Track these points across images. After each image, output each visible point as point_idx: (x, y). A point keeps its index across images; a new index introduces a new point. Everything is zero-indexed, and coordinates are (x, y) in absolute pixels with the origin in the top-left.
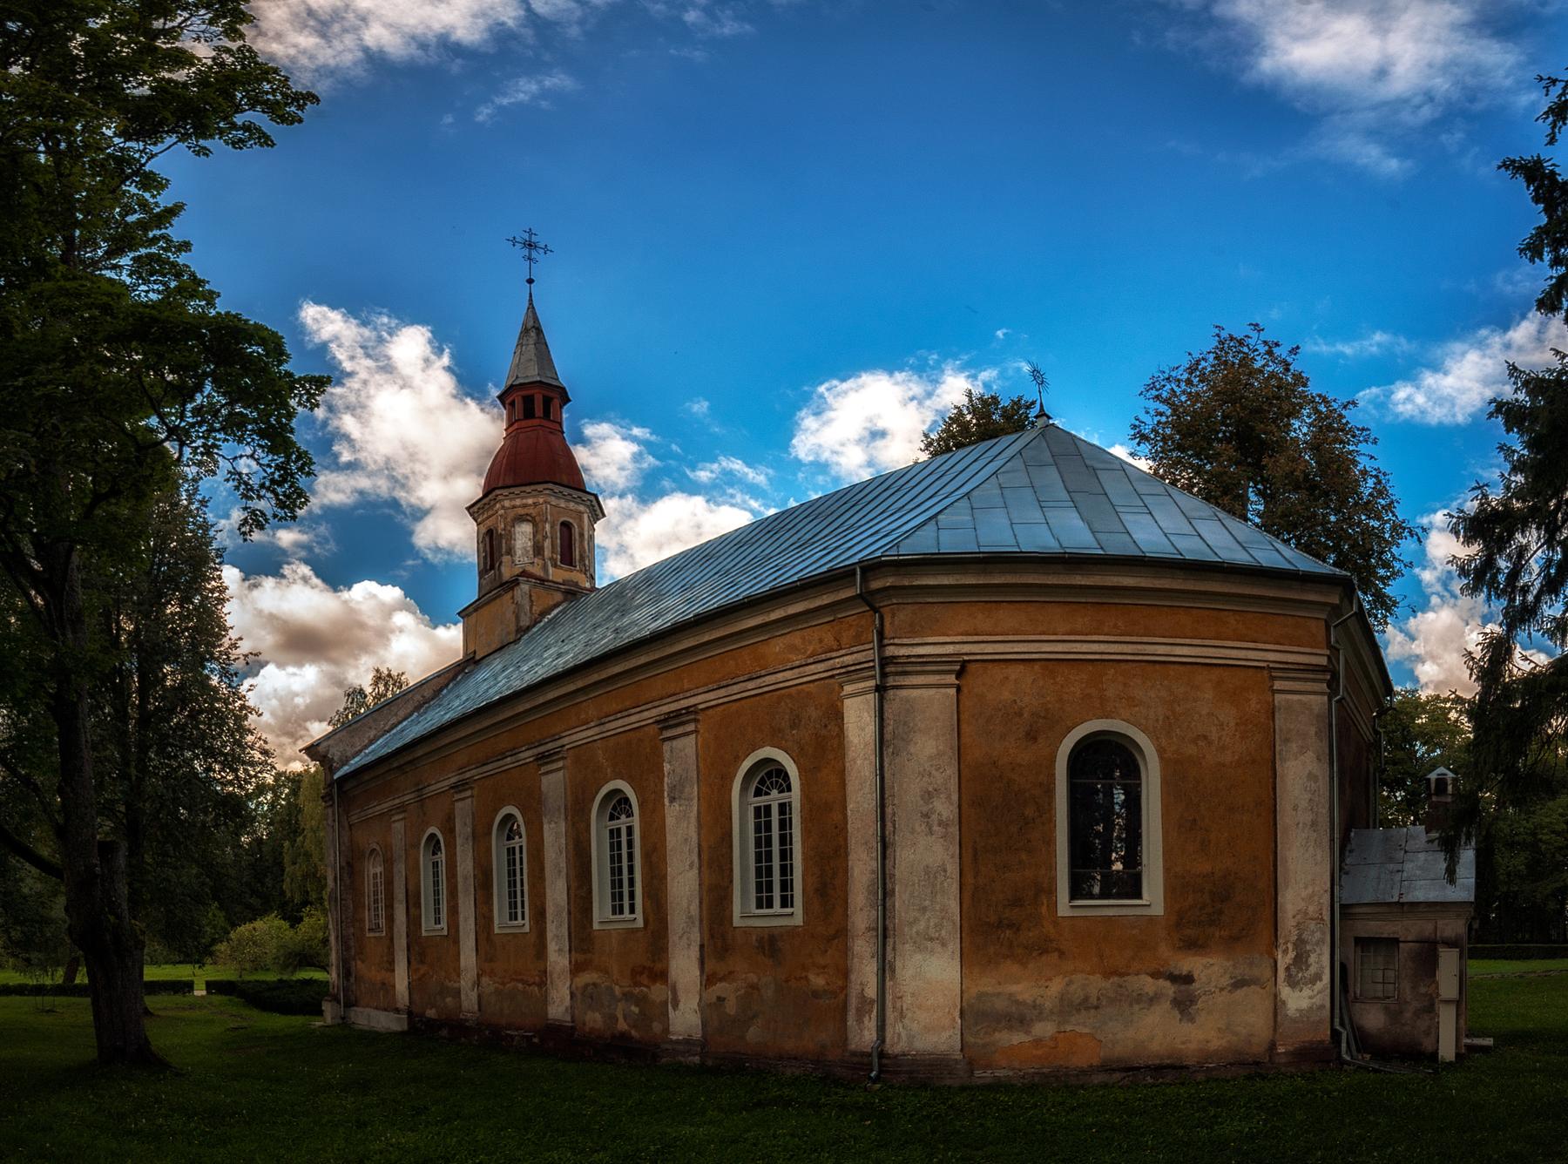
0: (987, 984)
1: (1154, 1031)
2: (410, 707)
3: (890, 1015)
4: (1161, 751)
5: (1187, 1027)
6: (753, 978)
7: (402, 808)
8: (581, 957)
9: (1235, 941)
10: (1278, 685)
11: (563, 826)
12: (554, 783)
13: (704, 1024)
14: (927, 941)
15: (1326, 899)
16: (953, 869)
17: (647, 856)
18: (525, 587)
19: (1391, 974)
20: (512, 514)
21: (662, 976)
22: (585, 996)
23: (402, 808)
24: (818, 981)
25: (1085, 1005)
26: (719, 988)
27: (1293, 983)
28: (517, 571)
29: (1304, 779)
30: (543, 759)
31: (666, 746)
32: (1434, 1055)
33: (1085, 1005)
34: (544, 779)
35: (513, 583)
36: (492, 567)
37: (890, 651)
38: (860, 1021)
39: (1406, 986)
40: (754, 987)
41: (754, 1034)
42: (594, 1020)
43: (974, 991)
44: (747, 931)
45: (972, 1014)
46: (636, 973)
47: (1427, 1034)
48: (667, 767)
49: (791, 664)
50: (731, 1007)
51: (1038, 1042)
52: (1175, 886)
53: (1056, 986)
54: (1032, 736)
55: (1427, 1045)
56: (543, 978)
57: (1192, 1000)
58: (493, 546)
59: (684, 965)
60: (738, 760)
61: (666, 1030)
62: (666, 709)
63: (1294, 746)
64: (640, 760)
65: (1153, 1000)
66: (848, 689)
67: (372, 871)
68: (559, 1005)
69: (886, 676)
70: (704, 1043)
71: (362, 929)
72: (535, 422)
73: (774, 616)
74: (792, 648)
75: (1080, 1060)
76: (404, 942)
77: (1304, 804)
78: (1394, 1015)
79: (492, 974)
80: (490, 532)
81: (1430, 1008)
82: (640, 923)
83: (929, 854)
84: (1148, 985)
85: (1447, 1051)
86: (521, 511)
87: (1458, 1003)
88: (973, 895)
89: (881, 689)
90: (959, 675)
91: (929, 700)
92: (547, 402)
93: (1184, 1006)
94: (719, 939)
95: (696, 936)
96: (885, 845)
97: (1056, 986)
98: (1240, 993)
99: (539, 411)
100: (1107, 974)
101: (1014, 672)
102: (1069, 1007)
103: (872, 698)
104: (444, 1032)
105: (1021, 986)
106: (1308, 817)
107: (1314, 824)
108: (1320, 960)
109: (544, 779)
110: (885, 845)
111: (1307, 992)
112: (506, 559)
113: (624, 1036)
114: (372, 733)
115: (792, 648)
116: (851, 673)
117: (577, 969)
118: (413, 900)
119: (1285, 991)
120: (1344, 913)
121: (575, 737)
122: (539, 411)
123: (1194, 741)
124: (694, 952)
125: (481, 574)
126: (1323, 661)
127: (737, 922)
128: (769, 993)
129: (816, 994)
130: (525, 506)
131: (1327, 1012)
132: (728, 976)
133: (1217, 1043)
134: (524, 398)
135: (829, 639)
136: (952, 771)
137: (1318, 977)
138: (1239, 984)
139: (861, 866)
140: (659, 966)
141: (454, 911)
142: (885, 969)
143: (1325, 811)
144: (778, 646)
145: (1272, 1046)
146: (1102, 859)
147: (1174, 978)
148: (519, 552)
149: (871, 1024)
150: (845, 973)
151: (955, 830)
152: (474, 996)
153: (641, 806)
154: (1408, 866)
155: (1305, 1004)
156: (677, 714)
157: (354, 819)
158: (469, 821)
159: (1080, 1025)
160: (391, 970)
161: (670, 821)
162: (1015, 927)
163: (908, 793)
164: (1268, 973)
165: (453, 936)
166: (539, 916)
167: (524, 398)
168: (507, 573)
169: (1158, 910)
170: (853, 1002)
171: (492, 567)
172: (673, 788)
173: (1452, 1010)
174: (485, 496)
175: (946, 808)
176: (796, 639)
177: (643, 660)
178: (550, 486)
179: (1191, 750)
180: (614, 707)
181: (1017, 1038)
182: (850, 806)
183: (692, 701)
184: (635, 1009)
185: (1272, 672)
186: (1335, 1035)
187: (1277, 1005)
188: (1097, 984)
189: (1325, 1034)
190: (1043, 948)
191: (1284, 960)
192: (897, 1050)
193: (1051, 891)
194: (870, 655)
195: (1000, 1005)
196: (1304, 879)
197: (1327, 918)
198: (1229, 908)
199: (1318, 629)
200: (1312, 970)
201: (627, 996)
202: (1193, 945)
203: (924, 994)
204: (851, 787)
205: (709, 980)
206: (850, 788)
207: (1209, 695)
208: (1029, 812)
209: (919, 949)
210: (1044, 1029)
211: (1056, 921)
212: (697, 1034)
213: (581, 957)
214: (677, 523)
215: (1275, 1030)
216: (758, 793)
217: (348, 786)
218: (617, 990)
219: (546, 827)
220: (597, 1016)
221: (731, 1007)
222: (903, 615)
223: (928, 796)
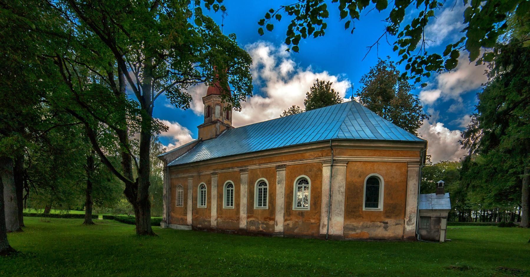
0: (348, 222)
1: (380, 232)
2: (186, 150)
3: (330, 228)
4: (384, 180)
5: (386, 232)
7: (192, 177)
8: (250, 215)
9: (396, 216)
10: (409, 166)
11: (247, 186)
12: (244, 177)
13: (284, 229)
14: (338, 214)
15: (416, 209)
16: (343, 201)
17: (270, 195)
18: (219, 124)
19: (428, 224)
20: (215, 102)
21: (273, 219)
22: (250, 223)
23: (192, 177)
24: (313, 221)
25: (367, 227)
26: (288, 222)
27: (408, 225)
28: (216, 119)
29: (413, 185)
30: (241, 171)
31: (278, 172)
32: (439, 241)
33: (367, 227)
34: (242, 176)
35: (215, 122)
36: (209, 116)
37: (335, 158)
38: (323, 228)
39: (432, 227)
40: (296, 222)
41: (296, 231)
42: (253, 228)
43: (346, 224)
44: (295, 211)
45: (345, 228)
46: (265, 219)
47: (437, 236)
48: (277, 177)
49: (311, 160)
50: (291, 226)
51: (357, 234)
52: (385, 205)
53: (361, 223)
54: (360, 176)
55: (437, 238)
56: (238, 219)
57: (387, 227)
58: (209, 111)
59: (280, 217)
60: (295, 177)
61: (274, 230)
62: (278, 164)
63: (411, 178)
64: (271, 175)
65: (380, 227)
66: (324, 165)
67: (178, 191)
68: (243, 224)
69: (333, 163)
70: (284, 233)
71: (174, 205)
73: (309, 148)
74: (311, 155)
75: (365, 237)
76: (191, 209)
77: (412, 190)
78: (429, 232)
79: (221, 217)
80: (209, 106)
81: (438, 231)
82: (267, 208)
83: (339, 198)
84: (379, 224)
85: (442, 239)
86: (217, 102)
87: (445, 230)
88: (347, 206)
89: (332, 166)
90: (347, 164)
91: (341, 169)
93: (386, 228)
94: (288, 211)
95: (283, 211)
96: (331, 196)
97: (361, 223)
98: (397, 226)
100: (371, 222)
101: (358, 164)
102: (363, 227)
103: (330, 167)
104: (205, 230)
105: (354, 223)
106: (413, 193)
107: (415, 194)
108: (414, 220)
109: (242, 176)
110: (331, 196)
111: (411, 226)
112: (213, 115)
113: (261, 231)
114: (177, 155)
115: (311, 155)
116: (325, 162)
117: (248, 217)
118: (195, 199)
119: (406, 226)
120: (420, 211)
123: (391, 178)
124: (282, 215)
125: (205, 117)
126: (419, 160)
127: (293, 209)
128: (301, 223)
129: (312, 224)
131: (415, 231)
132: (291, 220)
133: (391, 235)
135: (320, 154)
136: (344, 183)
137: (413, 224)
138: (397, 224)
139: (325, 200)
140: (272, 217)
141: (209, 202)
142: (329, 219)
143: (417, 191)
144: (308, 154)
145: (403, 236)
146: (372, 199)
147: (384, 223)
148: (216, 114)
150: (320, 220)
151: (344, 194)
152: (216, 222)
153: (269, 184)
154: (433, 202)
155: (410, 229)
156: (282, 165)
157: (173, 177)
158: (216, 182)
159: (365, 231)
160: (186, 214)
161: (277, 188)
162: (354, 212)
163: (336, 186)
164: (403, 223)
165: (209, 209)
166: (238, 205)
168: (213, 119)
169: (382, 210)
170: (321, 225)
171: (209, 116)
172: (279, 181)
173: (444, 232)
175: (343, 190)
176: (312, 153)
177: (274, 153)
179: (390, 179)
180: (264, 162)
181: (353, 233)
182: (323, 188)
183: (285, 163)
184: (265, 226)
185: (408, 163)
186: (416, 235)
187: (404, 229)
188: (369, 223)
189: (414, 235)
190: (360, 216)
191: (406, 220)
192: (331, 234)
193: (362, 206)
194: (330, 159)
195: (351, 226)
196: (412, 204)
197: (416, 212)
198: (397, 210)
199: (418, 153)
200: (412, 222)
201: (263, 223)
202: (388, 217)
203: (335, 224)
204: (323, 184)
205: (285, 220)
206: (323, 185)
207: (395, 168)
208: (359, 191)
209: (336, 215)
210: (358, 231)
211: (362, 211)
212: (282, 231)
213: (250, 215)
215: (404, 233)
216: (299, 184)
217: (171, 168)
218: (260, 222)
219: (241, 186)
220: (254, 227)
221: (291, 226)
222: (337, 151)
223: (340, 187)
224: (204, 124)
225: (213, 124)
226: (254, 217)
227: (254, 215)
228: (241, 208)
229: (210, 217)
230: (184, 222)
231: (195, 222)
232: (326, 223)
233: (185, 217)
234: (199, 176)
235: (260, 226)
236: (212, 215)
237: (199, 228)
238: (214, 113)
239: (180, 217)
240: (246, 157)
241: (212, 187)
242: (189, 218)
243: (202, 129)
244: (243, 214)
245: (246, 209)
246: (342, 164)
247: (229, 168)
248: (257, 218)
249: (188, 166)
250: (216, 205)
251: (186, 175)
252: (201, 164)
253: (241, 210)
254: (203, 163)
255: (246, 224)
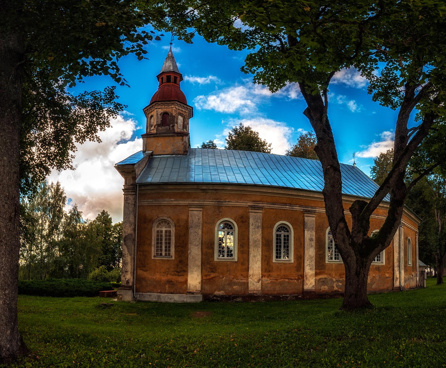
6: (374, 275)
8: (318, 271)
38: (396, 281)
40: (374, 277)
41: (374, 286)
42: (325, 288)
56: (302, 277)
68: (310, 283)
72: (171, 84)
92: (175, 78)
99: (172, 80)
104: (239, 299)
113: (336, 291)
117: (316, 274)
121: (321, 210)
122: (172, 80)
129: (387, 278)
130: (182, 111)
134: (167, 76)
149: (398, 282)
167: (167, 76)
174: (150, 105)
178: (177, 102)
201: (337, 281)
213: (318, 271)
214: (118, 97)
218: (334, 279)
220: (326, 287)
224: (156, 134)
225: (180, 136)
226: (326, 274)
227: (326, 272)
228: (307, 263)
229: (247, 276)
230: (182, 288)
231: (207, 287)
232: (398, 276)
233: (181, 279)
234: (219, 207)
235: (335, 285)
236: (251, 272)
237: (222, 297)
238: (177, 123)
239: (164, 278)
240: (275, 191)
241: (251, 227)
242: (194, 280)
243: (152, 140)
244: (309, 270)
245: (313, 263)
246: (197, 209)
247: (285, 204)
248: (330, 275)
249: (195, 187)
250: (259, 257)
251: (186, 202)
252: (229, 188)
253: (306, 264)
254: (156, 187)
255: (314, 284)
